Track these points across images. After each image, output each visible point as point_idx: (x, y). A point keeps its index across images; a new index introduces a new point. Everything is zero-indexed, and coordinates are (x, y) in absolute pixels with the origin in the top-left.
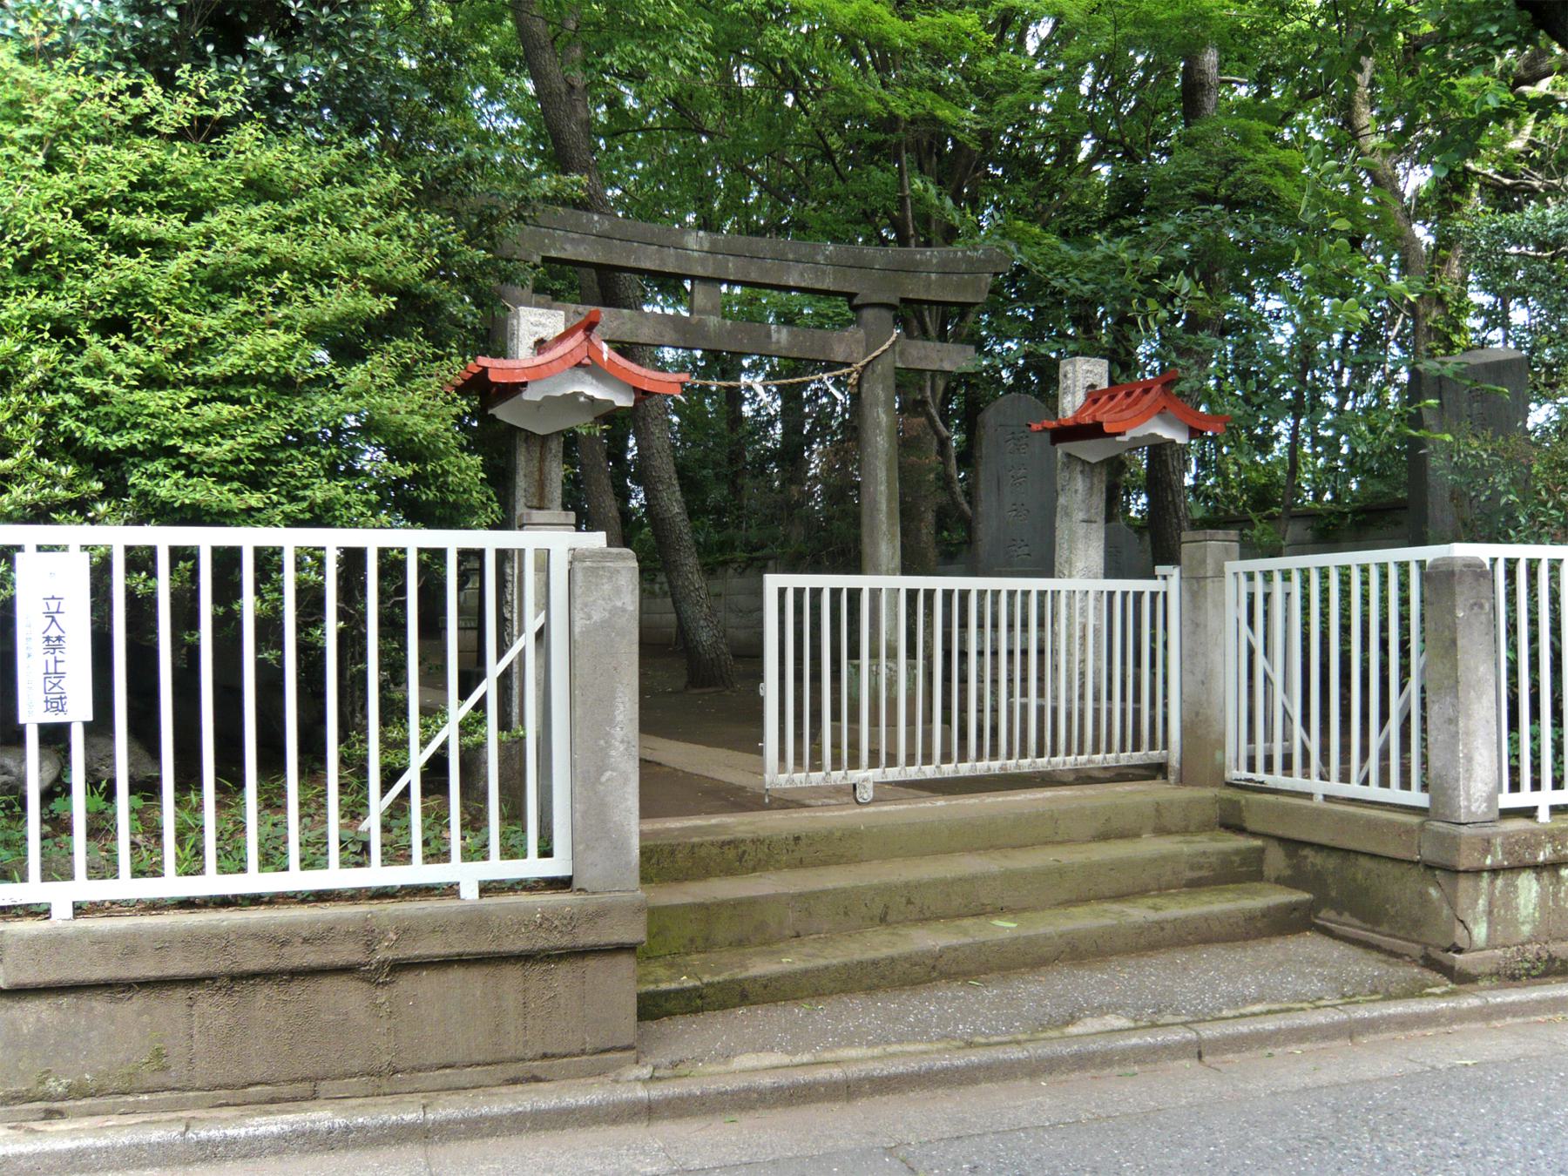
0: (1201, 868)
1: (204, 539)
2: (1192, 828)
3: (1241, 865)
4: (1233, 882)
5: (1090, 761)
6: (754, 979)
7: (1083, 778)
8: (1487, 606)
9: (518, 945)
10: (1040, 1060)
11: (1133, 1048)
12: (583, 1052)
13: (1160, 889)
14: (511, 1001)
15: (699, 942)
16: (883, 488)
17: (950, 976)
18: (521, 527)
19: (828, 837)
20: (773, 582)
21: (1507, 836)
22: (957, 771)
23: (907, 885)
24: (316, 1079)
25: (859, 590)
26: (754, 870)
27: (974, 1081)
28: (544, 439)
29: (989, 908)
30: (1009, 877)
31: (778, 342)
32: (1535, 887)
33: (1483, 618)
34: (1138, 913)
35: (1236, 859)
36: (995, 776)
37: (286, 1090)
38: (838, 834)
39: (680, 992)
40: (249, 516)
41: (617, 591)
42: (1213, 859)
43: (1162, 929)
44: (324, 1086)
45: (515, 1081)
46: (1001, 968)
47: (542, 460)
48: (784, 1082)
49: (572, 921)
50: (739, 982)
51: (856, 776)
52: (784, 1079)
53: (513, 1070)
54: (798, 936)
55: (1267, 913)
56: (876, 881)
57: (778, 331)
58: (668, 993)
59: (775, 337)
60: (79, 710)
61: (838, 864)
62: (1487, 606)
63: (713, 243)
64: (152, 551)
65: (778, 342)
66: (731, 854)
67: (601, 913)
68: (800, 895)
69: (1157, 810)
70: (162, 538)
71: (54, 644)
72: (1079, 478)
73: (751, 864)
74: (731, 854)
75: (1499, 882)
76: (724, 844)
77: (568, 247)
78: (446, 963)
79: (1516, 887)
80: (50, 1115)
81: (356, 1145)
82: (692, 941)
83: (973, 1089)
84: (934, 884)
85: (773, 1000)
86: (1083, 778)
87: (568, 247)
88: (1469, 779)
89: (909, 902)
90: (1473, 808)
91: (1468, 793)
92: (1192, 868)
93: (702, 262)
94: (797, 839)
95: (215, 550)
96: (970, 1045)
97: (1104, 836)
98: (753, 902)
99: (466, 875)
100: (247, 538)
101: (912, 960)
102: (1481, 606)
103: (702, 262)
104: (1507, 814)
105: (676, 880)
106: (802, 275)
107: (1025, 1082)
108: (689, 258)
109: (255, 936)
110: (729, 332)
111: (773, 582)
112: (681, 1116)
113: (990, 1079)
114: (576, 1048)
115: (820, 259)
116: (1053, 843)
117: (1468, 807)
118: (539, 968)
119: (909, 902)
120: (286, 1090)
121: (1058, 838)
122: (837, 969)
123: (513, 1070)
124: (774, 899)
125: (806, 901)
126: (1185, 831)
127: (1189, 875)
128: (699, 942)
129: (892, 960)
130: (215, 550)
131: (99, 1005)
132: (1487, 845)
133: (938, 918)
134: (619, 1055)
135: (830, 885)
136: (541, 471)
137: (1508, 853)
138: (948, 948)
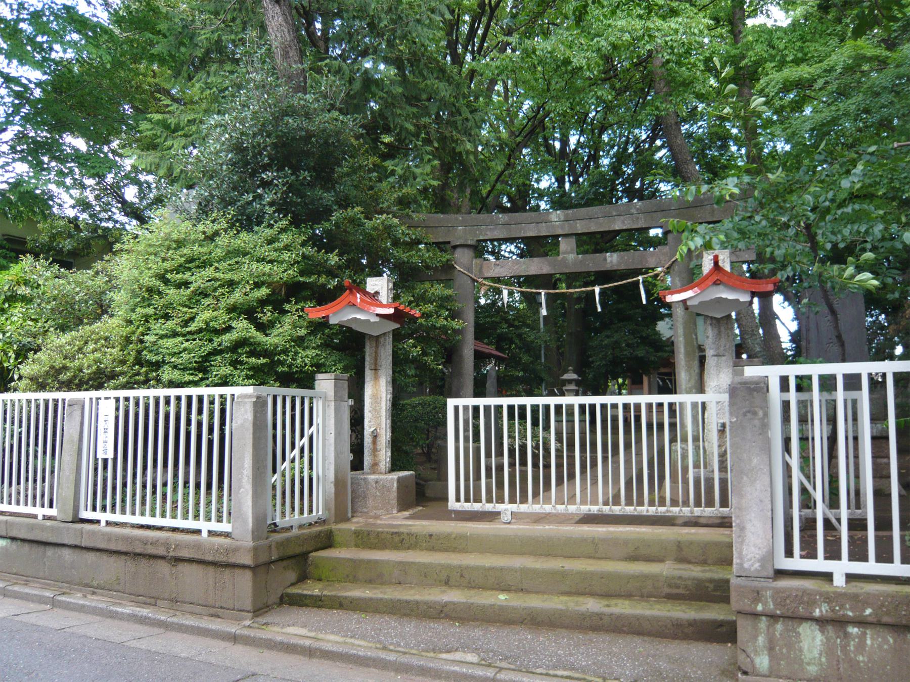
0: (678, 587)
1: (183, 392)
2: (709, 562)
3: (715, 590)
4: (696, 600)
5: (667, 511)
6: (346, 598)
7: (694, 523)
8: (761, 414)
9: (210, 558)
10: (401, 664)
11: (454, 672)
12: (234, 609)
13: (642, 596)
14: (211, 582)
15: (351, 578)
16: (681, 339)
17: (448, 617)
18: (232, 385)
19: (448, 536)
20: (451, 403)
21: (777, 591)
22: (692, 512)
23: (460, 566)
24: (157, 598)
25: (501, 406)
26: (408, 548)
27: (368, 666)
28: (377, 338)
29: (513, 588)
30: (524, 571)
31: (611, 262)
32: (819, 637)
33: (757, 422)
34: (592, 605)
35: (711, 586)
36: (595, 515)
37: (148, 600)
38: (454, 536)
39: (311, 596)
40: (196, 384)
41: (246, 411)
42: (689, 583)
43: (601, 619)
44: (158, 602)
45: (212, 616)
46: (483, 620)
47: (377, 347)
48: (285, 641)
49: (228, 551)
50: (338, 597)
51: (500, 507)
52: (340, 649)
53: (212, 611)
54: (400, 583)
55: (693, 623)
56: (443, 562)
57: (611, 256)
58: (306, 596)
59: (609, 260)
60: (110, 455)
61: (454, 551)
62: (761, 414)
63: (566, 216)
64: (833, 377)
65: (611, 262)
66: (397, 539)
67: (236, 550)
68: (400, 563)
69: (678, 546)
70: (173, 392)
71: (106, 430)
72: (710, 328)
73: (407, 545)
74: (397, 539)
75: (779, 627)
76: (393, 533)
77: (488, 233)
78: (191, 561)
79: (798, 634)
80: (94, 593)
81: (147, 624)
82: (348, 576)
83: (366, 670)
84: (477, 568)
85: (354, 609)
86: (694, 523)
87: (488, 233)
88: (742, 543)
89: (462, 576)
90: (746, 565)
91: (740, 553)
92: (670, 586)
93: (562, 227)
94: (431, 536)
95: (895, 374)
96: (385, 648)
97: (634, 558)
98: (376, 562)
99: (204, 526)
100: (194, 391)
101: (430, 605)
102: (755, 413)
103: (562, 227)
104: (781, 574)
105: (370, 548)
106: (623, 222)
107: (393, 674)
108: (553, 226)
109: (139, 540)
110: (581, 262)
111: (451, 403)
112: (246, 644)
113: (375, 667)
114: (231, 607)
115: (634, 211)
116: (594, 558)
117: (741, 565)
118: (220, 569)
119: (462, 576)
120: (148, 600)
121: (597, 555)
122: (387, 601)
123: (212, 611)
124: (387, 562)
125: (404, 566)
126: (704, 562)
127: (667, 590)
128: (351, 578)
129: (417, 602)
130: (895, 374)
131: (105, 557)
132: (757, 595)
133: (479, 588)
134: (246, 614)
135: (417, 560)
136: (376, 352)
137: (780, 603)
138: (450, 602)
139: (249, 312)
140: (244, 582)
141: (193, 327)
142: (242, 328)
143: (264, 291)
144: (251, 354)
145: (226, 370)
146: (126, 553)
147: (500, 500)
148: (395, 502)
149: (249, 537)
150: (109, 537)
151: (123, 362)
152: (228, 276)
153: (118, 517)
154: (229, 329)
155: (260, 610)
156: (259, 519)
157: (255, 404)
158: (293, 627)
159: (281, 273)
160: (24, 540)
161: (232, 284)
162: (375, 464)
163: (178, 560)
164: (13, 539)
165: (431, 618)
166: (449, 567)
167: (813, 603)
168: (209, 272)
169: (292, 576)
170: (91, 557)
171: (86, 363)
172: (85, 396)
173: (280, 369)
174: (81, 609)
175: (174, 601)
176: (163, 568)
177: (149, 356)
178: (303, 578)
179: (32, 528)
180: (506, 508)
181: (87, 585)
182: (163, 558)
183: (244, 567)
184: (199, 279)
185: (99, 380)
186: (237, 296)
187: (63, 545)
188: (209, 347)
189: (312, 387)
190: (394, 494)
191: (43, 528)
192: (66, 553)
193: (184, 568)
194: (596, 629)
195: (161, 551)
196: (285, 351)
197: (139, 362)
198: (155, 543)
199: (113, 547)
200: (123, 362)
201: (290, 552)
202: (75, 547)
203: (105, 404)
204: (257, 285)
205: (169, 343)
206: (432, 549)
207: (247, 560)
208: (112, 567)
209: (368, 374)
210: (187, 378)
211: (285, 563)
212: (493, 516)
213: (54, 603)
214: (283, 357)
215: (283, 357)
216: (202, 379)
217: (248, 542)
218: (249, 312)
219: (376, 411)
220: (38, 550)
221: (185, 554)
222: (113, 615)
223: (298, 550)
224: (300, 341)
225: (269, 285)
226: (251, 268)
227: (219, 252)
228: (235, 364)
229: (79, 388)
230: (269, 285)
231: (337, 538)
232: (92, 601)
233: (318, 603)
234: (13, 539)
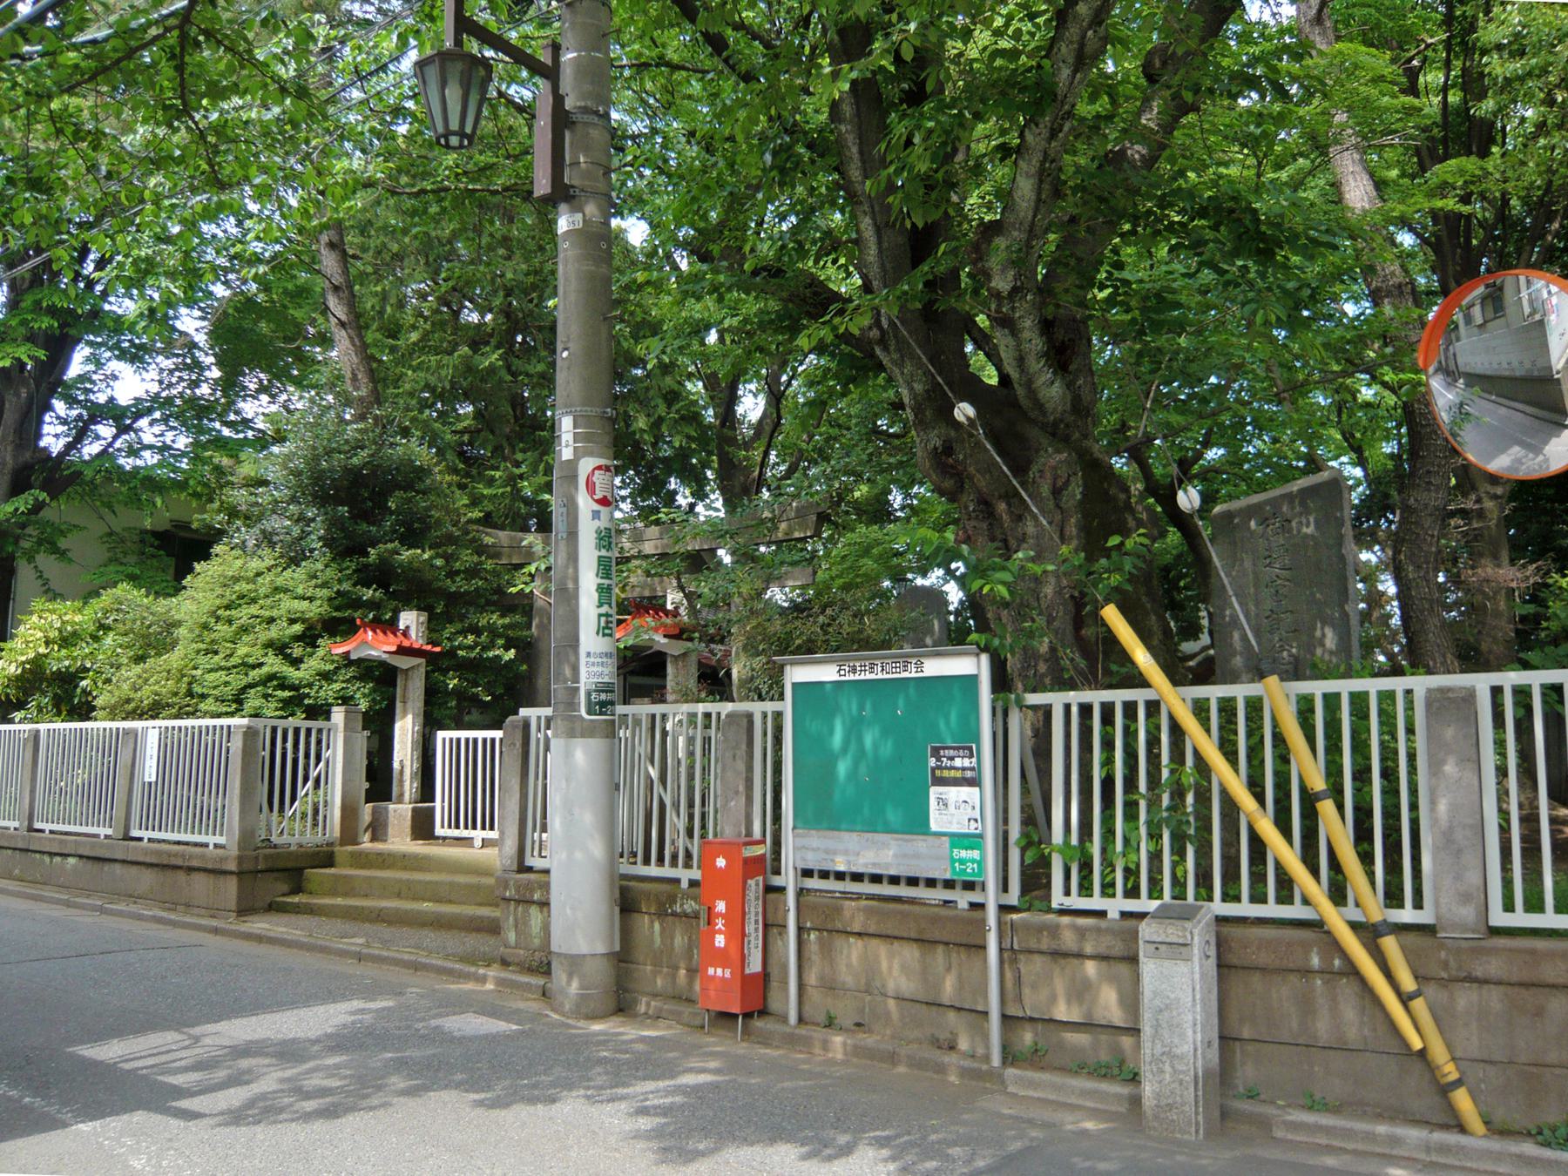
9: (210, 866)
20: (441, 734)
21: (517, 881)
84: (420, 882)
101: (371, 910)
131: (143, 868)
139: (280, 648)
140: (231, 886)
141: (234, 661)
142: (273, 664)
143: (298, 628)
144: (282, 687)
145: (258, 703)
146: (156, 865)
147: (474, 828)
148: (408, 830)
149: (236, 847)
150: (146, 852)
151: (176, 694)
152: (267, 614)
153: (156, 835)
154: (261, 665)
155: (244, 911)
156: (246, 836)
157: (245, 734)
158: (259, 924)
159: (314, 610)
160: (88, 858)
161: (271, 620)
162: (402, 795)
163: (191, 870)
164: (81, 857)
165: (371, 921)
166: (400, 881)
167: (532, 891)
168: (253, 609)
169: (285, 888)
170: (134, 870)
171: (146, 695)
172: (137, 724)
173: (306, 702)
174: (120, 914)
175: (187, 905)
176: (181, 877)
177: (198, 689)
178: (297, 890)
179: (93, 846)
180: (478, 835)
181: (131, 896)
182: (180, 868)
183: (231, 873)
184: (244, 614)
185: (154, 710)
186: (273, 633)
187: (115, 861)
188: (244, 683)
189: (328, 718)
190: (409, 823)
191: (102, 845)
192: (117, 866)
193: (197, 876)
194: (478, 930)
195: (179, 862)
196: (310, 685)
197: (190, 693)
198: (169, 854)
199: (148, 860)
200: (176, 694)
201: (281, 865)
202: (124, 861)
203: (151, 732)
204: (292, 621)
205: (211, 677)
206: (405, 868)
207: (232, 867)
208: (147, 878)
209: (399, 705)
210: (225, 709)
211: (275, 875)
212: (466, 842)
213: (102, 910)
214: (307, 691)
215: (307, 691)
216: (237, 710)
217: (234, 851)
218: (280, 648)
219: (403, 742)
220: (97, 866)
221: (195, 863)
222: (140, 918)
223: (290, 865)
224: (326, 676)
225: (304, 621)
226: (289, 604)
227: (262, 591)
228: (266, 696)
229: (140, 717)
230: (304, 621)
231: (338, 859)
232: (133, 908)
233: (310, 910)
234: (81, 857)
